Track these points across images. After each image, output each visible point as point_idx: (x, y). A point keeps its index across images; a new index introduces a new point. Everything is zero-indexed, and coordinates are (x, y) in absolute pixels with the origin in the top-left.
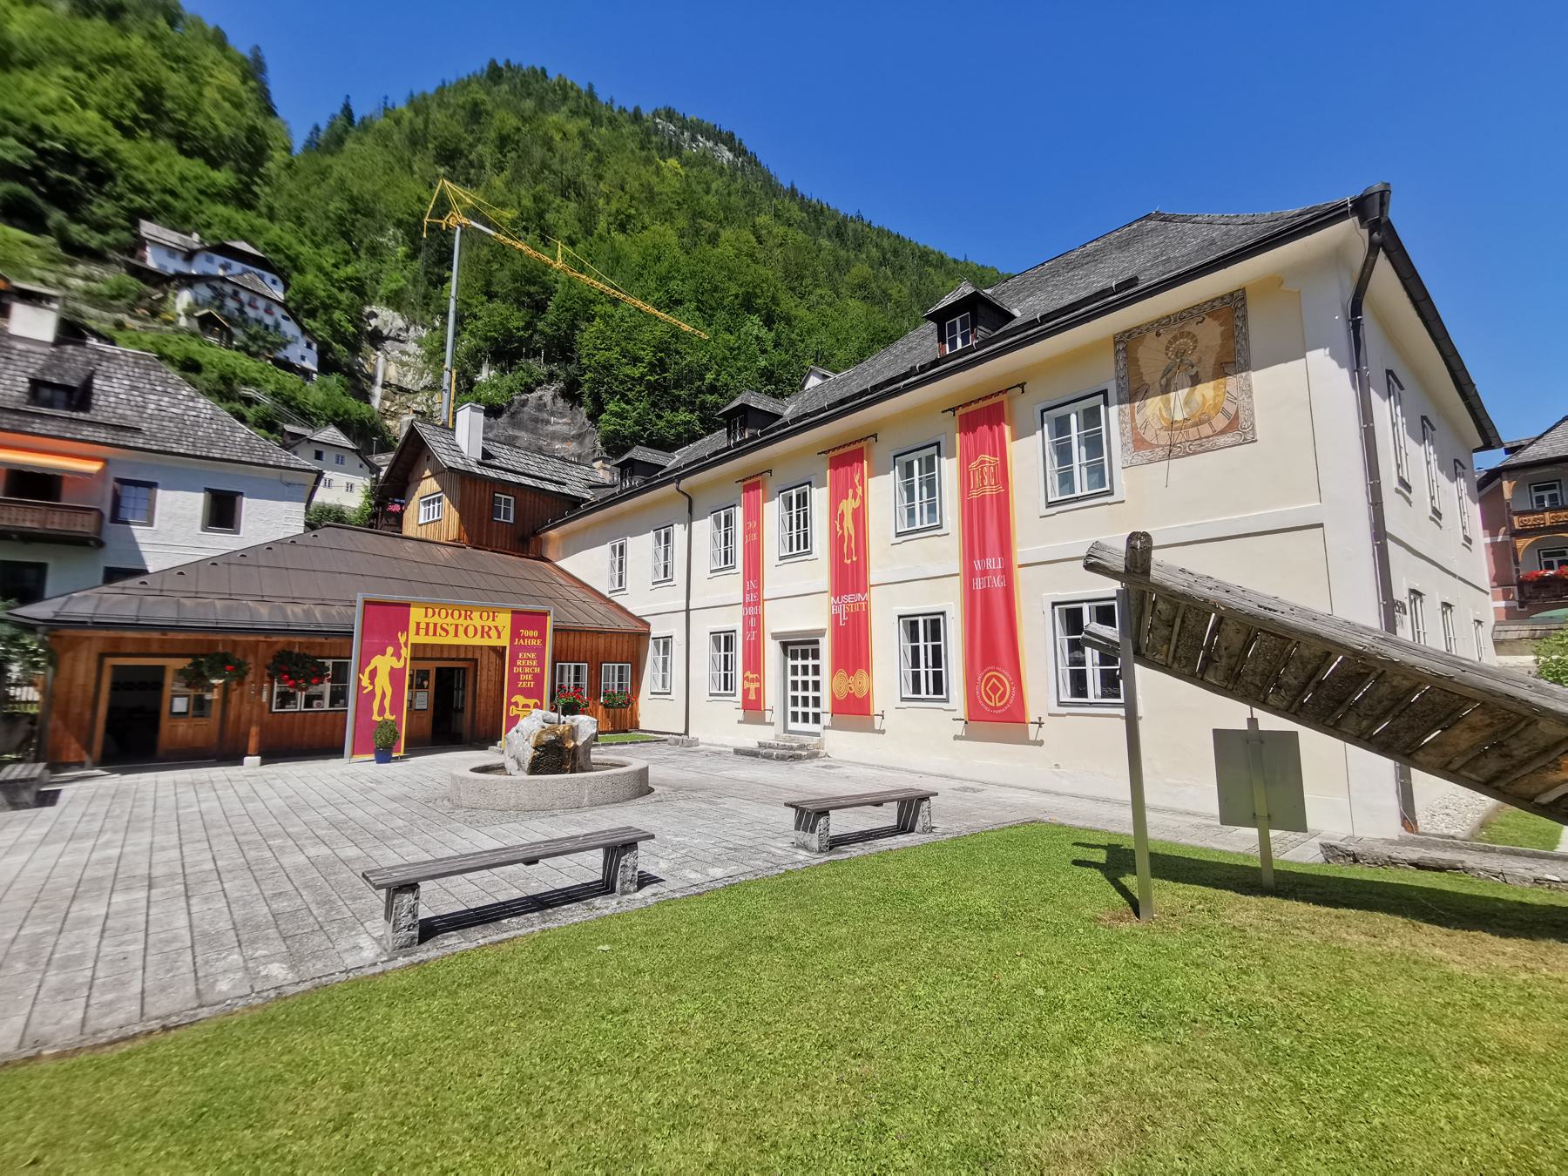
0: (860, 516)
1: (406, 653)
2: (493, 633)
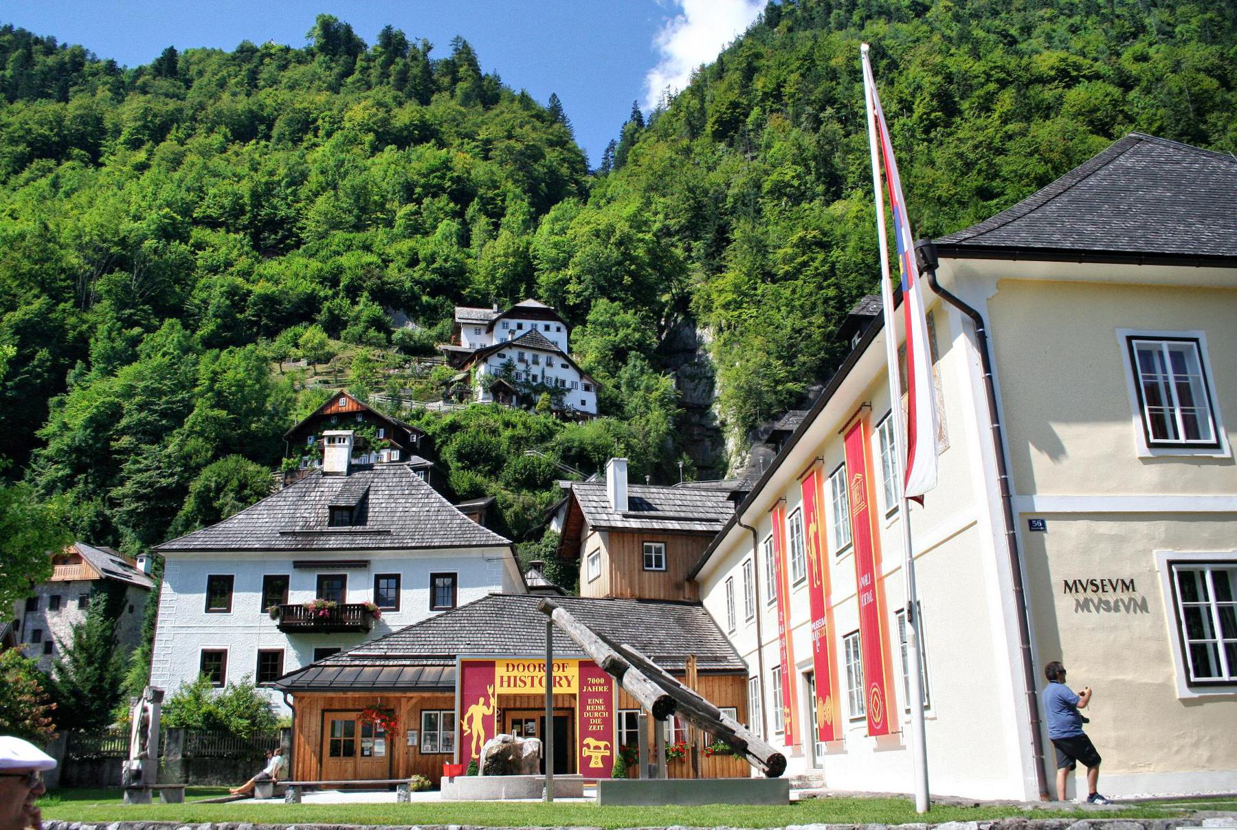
1: (494, 702)
2: (564, 682)
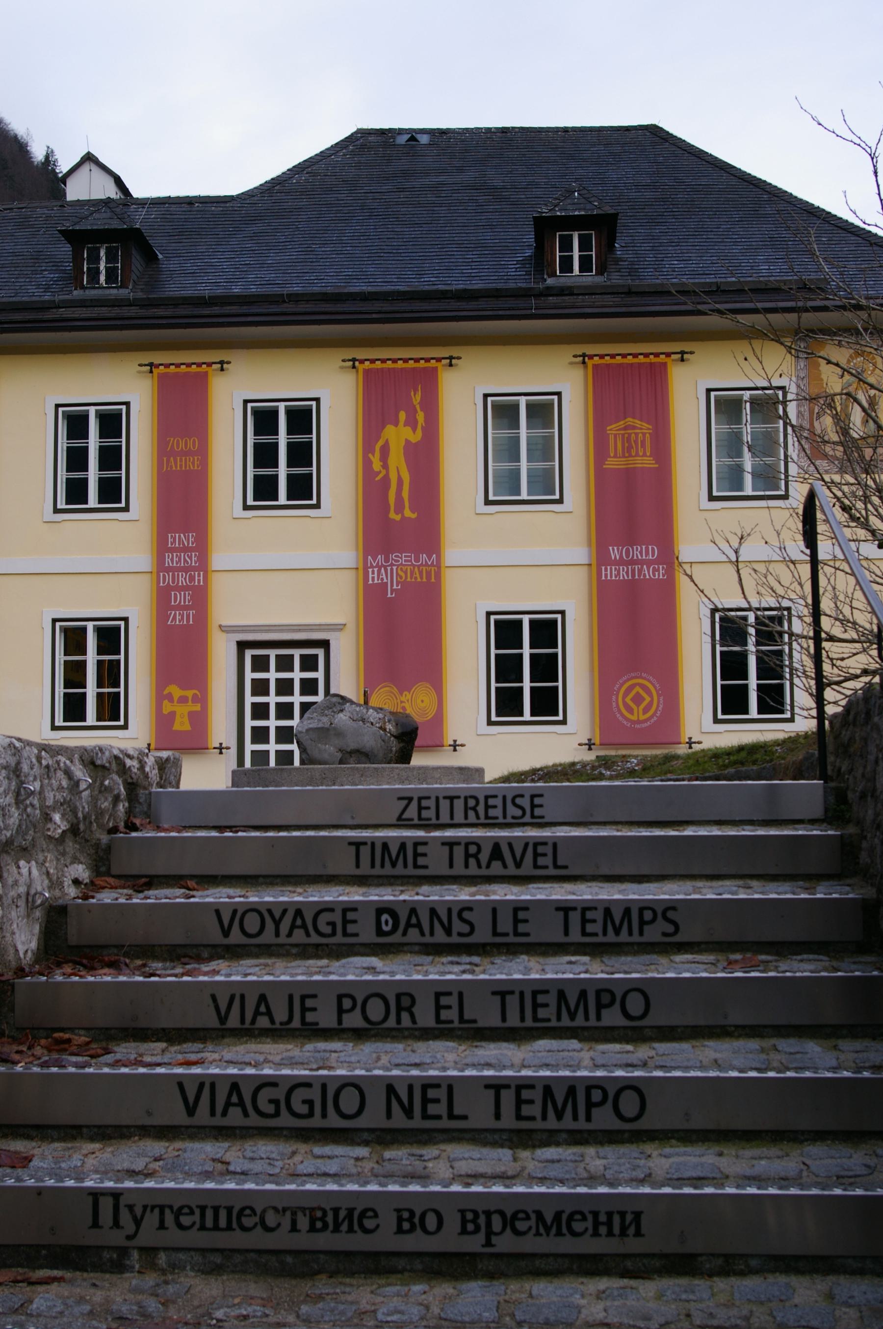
0: (425, 459)
